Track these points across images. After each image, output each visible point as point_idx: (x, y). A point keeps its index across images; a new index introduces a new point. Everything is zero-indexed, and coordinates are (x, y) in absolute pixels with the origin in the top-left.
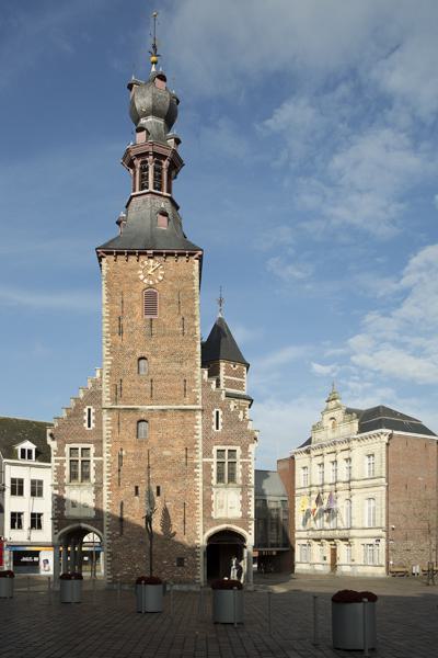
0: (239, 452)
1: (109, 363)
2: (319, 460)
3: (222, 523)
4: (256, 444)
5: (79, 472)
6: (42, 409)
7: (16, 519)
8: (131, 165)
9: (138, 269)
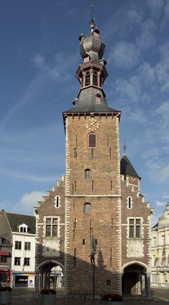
0: (142, 220)
1: (69, 172)
2: (163, 234)
3: (131, 261)
4: (152, 216)
5: (51, 232)
6: (29, 203)
7: (17, 261)
8: (81, 76)
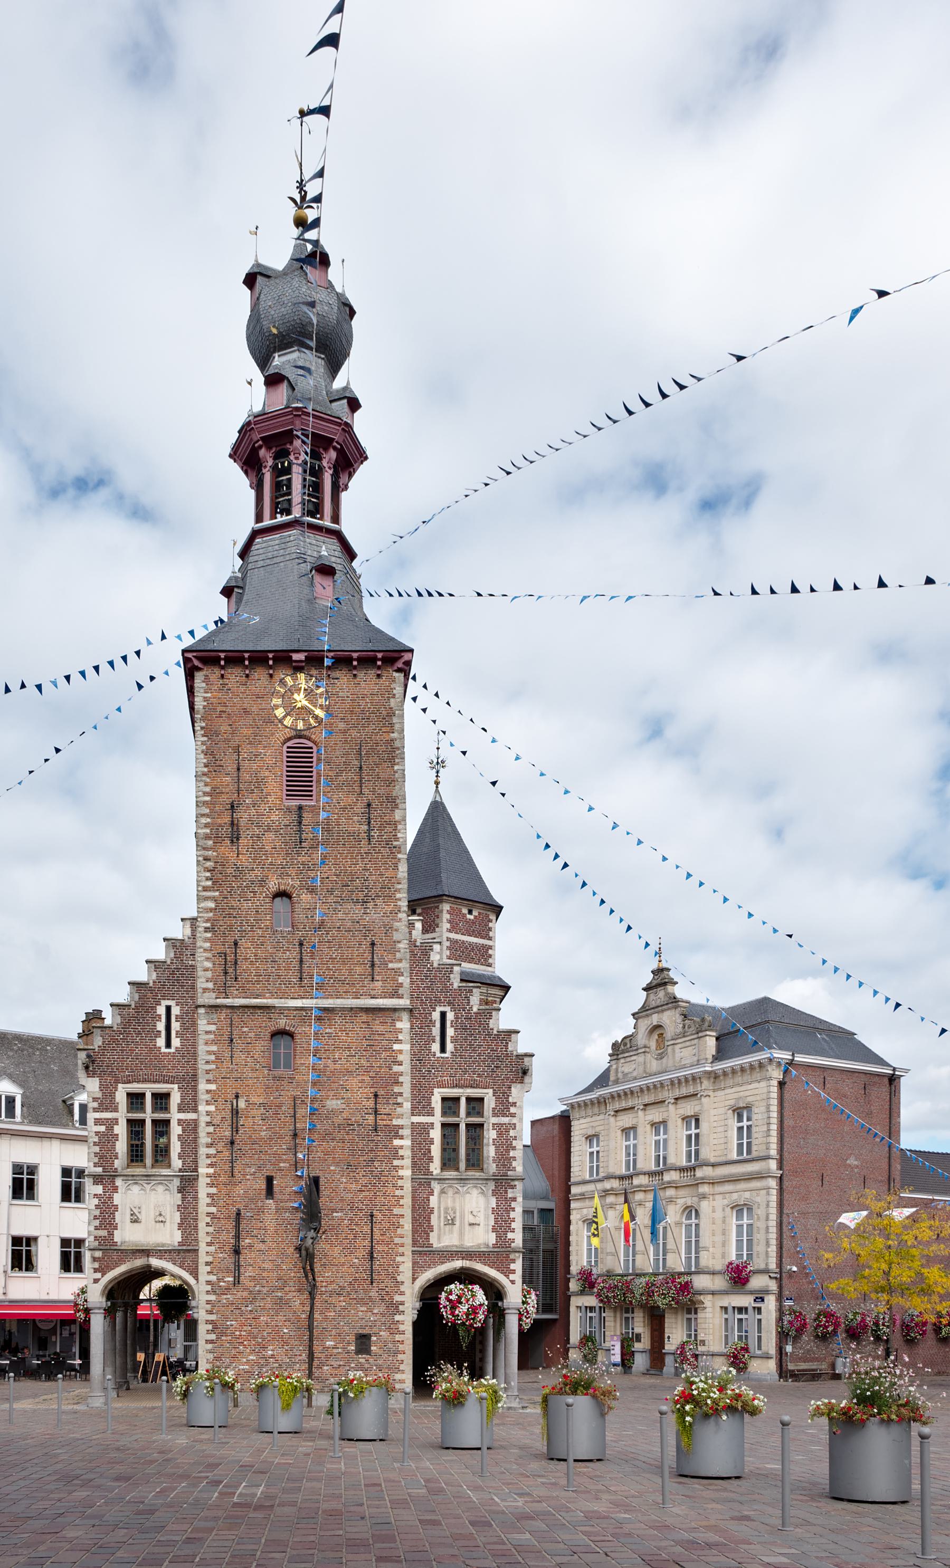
0: (490, 1102)
9: (274, 693)
